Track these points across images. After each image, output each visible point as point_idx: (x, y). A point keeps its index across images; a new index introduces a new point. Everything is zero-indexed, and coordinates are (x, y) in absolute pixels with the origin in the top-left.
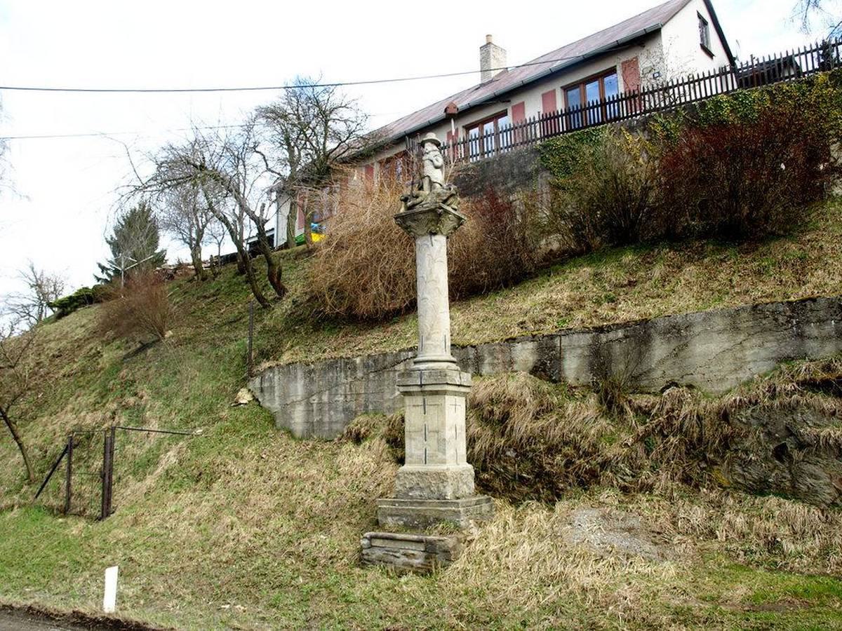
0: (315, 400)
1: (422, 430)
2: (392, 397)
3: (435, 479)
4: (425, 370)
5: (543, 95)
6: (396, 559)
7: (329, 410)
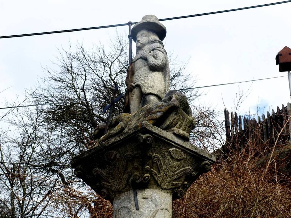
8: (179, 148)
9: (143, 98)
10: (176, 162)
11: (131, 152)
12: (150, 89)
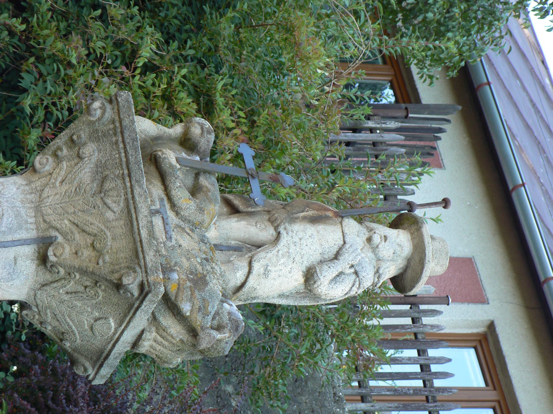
8: (114, 334)
9: (249, 246)
10: (88, 323)
11: (111, 249)
12: (262, 269)
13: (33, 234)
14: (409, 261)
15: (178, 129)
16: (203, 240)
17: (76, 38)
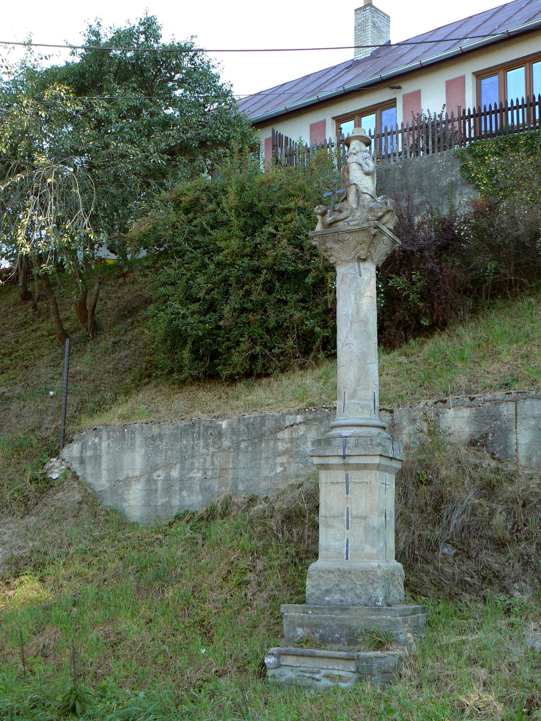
0: (160, 475)
1: (343, 515)
2: (272, 474)
3: (362, 580)
4: (350, 437)
5: (449, 84)
6: (317, 683)
7: (181, 490)
13: (356, 263)
14: (361, 141)
15: (319, 217)
16: (357, 209)
17: (267, 253)
